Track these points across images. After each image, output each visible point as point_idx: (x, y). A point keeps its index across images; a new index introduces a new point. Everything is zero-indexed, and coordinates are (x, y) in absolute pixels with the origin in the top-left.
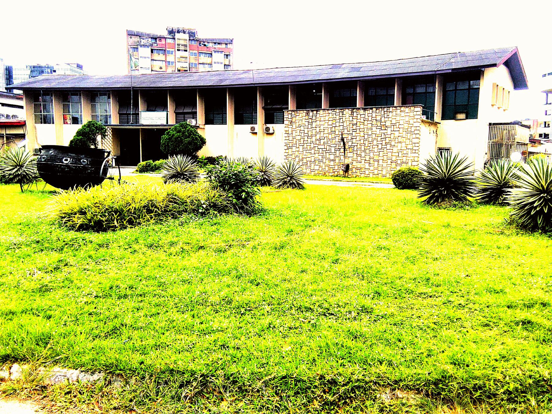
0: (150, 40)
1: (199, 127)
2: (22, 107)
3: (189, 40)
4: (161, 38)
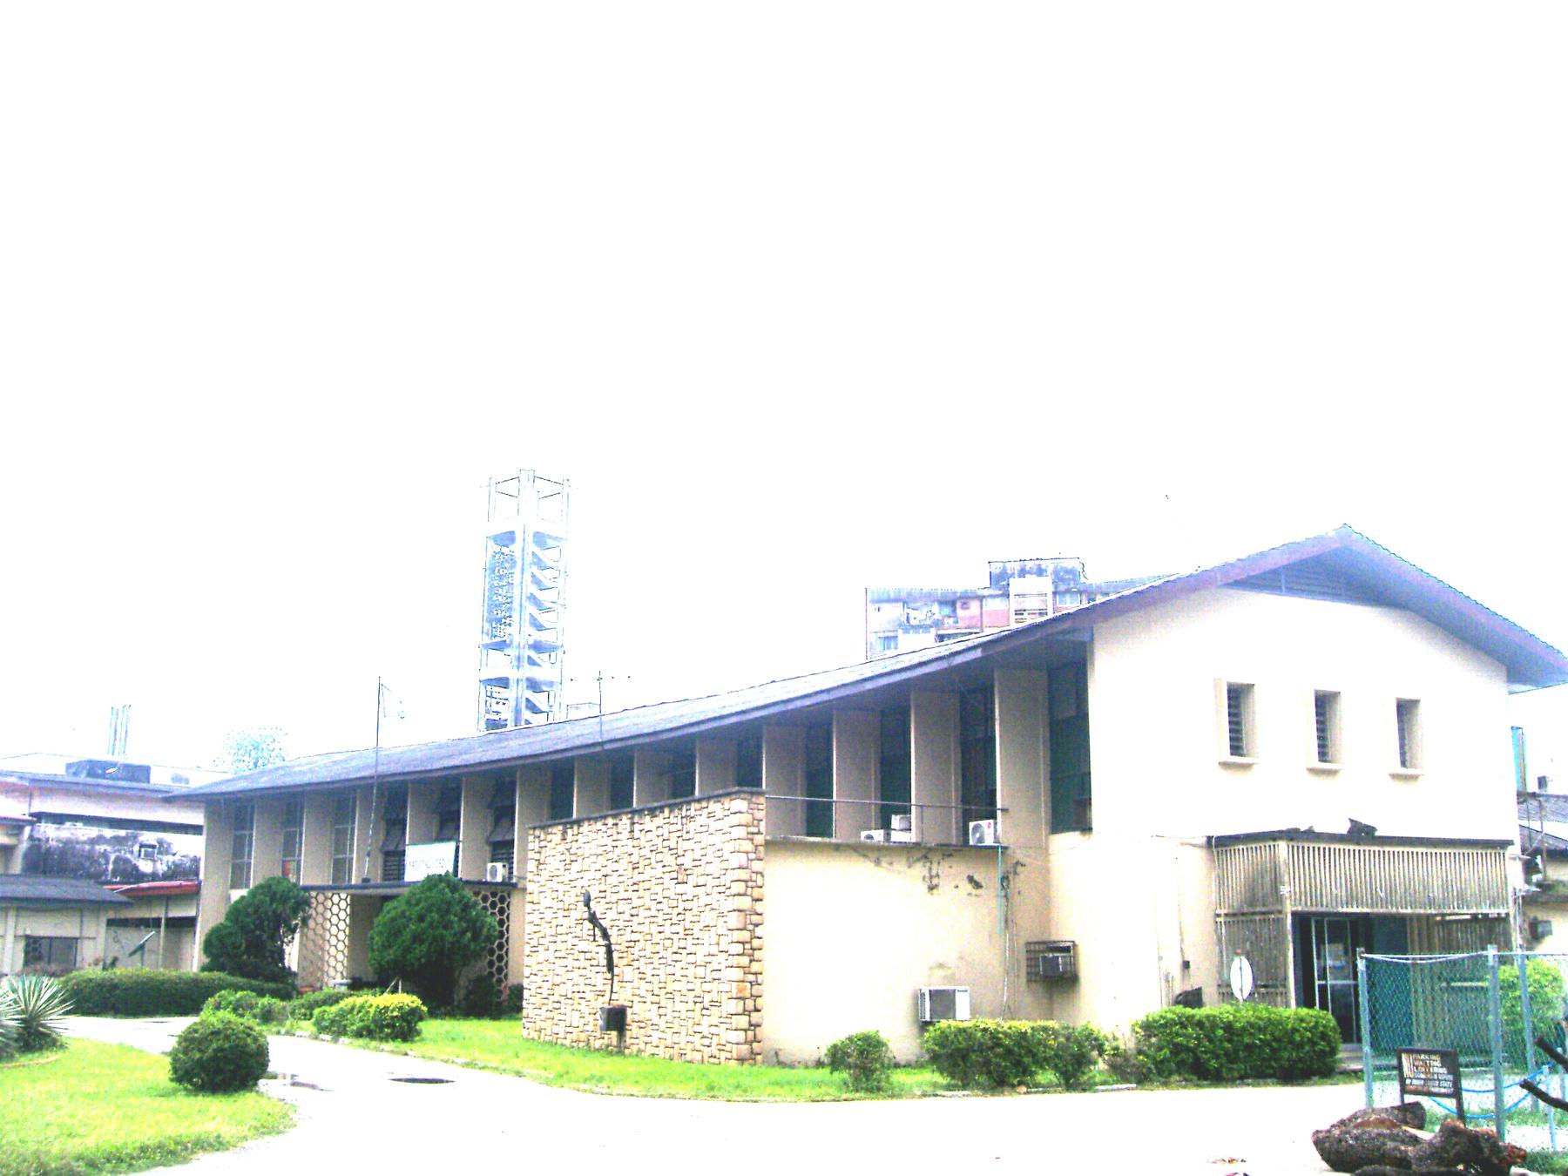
0: (936, 608)
2: (196, 830)
3: (1055, 593)
4: (966, 598)
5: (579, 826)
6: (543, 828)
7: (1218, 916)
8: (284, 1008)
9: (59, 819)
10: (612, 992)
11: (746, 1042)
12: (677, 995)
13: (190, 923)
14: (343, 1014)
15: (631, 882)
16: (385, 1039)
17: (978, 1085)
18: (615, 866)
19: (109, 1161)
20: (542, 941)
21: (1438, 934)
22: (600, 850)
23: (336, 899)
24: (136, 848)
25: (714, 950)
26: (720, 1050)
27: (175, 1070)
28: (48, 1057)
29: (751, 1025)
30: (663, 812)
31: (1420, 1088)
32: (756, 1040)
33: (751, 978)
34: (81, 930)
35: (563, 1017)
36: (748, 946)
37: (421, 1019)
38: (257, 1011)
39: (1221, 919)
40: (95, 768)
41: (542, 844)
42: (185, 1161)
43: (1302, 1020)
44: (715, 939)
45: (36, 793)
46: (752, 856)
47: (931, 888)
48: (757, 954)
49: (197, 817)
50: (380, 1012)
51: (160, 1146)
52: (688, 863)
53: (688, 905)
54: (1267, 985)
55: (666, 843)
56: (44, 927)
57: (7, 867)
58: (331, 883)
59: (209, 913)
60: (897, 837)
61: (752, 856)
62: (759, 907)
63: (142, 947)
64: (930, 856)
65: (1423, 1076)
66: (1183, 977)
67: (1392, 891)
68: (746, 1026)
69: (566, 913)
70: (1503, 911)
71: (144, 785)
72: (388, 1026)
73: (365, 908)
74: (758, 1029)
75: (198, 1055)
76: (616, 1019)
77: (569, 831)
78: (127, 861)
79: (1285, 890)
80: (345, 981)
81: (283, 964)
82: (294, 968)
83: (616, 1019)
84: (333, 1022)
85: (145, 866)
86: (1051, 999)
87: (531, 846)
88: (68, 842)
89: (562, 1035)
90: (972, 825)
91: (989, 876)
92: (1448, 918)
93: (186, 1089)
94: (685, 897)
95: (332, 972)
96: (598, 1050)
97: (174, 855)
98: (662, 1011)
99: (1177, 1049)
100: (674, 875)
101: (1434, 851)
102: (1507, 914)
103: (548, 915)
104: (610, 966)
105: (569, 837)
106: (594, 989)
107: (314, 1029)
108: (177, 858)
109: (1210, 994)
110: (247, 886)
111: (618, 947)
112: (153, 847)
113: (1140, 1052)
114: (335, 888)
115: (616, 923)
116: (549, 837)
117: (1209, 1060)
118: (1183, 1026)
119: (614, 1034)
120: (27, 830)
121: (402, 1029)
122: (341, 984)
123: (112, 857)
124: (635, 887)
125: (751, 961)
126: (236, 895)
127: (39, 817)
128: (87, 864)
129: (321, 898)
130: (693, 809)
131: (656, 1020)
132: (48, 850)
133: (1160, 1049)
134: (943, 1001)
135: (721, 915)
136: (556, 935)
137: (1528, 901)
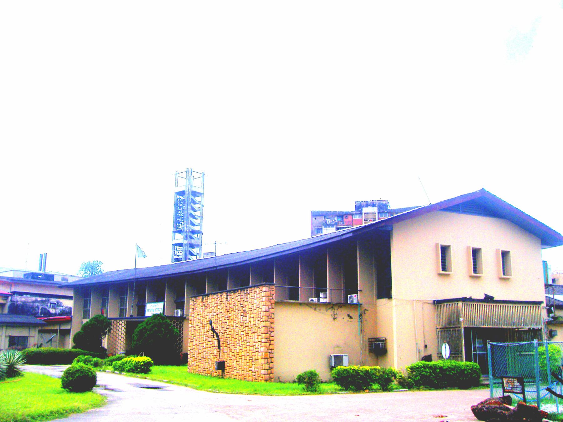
1: (185, 317)
2: (70, 298)
3: (379, 213)
5: (208, 296)
6: (195, 297)
7: (437, 329)
8: (102, 362)
9: (21, 294)
10: (220, 356)
11: (268, 374)
12: (243, 357)
13: (68, 332)
14: (123, 364)
15: (226, 316)
16: (139, 372)
17: (351, 389)
18: (221, 311)
19: (39, 416)
20: (195, 338)
21: (516, 335)
22: (215, 305)
23: (121, 322)
24: (49, 304)
25: (257, 340)
26: (259, 377)
27: (63, 384)
28: (16, 379)
29: (270, 368)
30: (238, 291)
31: (510, 390)
32: (271, 373)
33: (270, 351)
34: (29, 334)
35: (202, 365)
36: (269, 339)
37: (151, 366)
38: (92, 363)
39: (439, 330)
40: (34, 275)
41: (195, 303)
42: (66, 417)
43: (467, 366)
44: (256, 337)
45: (13, 285)
46: (270, 307)
47: (334, 319)
48: (272, 342)
49: (71, 293)
50: (136, 363)
51: (58, 411)
52: (247, 309)
53: (247, 325)
54: (455, 353)
55: (239, 302)
56: (16, 332)
57: (2, 311)
58: (119, 317)
59: (75, 327)
60: (322, 300)
61: (270, 307)
62: (272, 325)
63: (51, 340)
64: (334, 307)
65: (511, 386)
66: (425, 351)
67: (500, 319)
68: (268, 368)
69: (203, 328)
70: (540, 327)
71: (52, 282)
72: (139, 368)
73: (130, 327)
74: (272, 369)
75: (71, 379)
76: (221, 366)
77: (204, 298)
78: (46, 309)
79: (461, 319)
80: (124, 352)
81: (102, 346)
82: (106, 347)
83: (221, 366)
84: (120, 367)
85: (52, 311)
86: (377, 359)
87: (191, 303)
88: (24, 302)
89: (201, 371)
90: (349, 296)
91: (355, 314)
92: (520, 329)
93: (67, 391)
94: (246, 322)
95: (119, 349)
96: (215, 377)
97: (63, 307)
98: (238, 363)
99: (422, 376)
100: (242, 314)
101: (515, 305)
102: (541, 328)
103: (197, 328)
104: (219, 346)
105: (204, 300)
106: (213, 355)
107: (113, 369)
108: (64, 307)
109: (434, 356)
110: (89, 318)
111: (222, 340)
112: (55, 304)
113: (409, 377)
114: (120, 319)
115: (221, 331)
116: (197, 300)
117: (434, 380)
118: (425, 368)
119: (220, 371)
120: (10, 298)
121: (144, 369)
122: (123, 353)
123: (40, 308)
124: (228, 318)
125: (270, 345)
126: (85, 321)
127: (14, 293)
128: (32, 310)
129: (115, 322)
130: (249, 291)
131: (235, 365)
132: (17, 305)
133: (416, 376)
134: (338, 359)
135: (259, 328)
136: (200, 335)
137: (549, 323)
